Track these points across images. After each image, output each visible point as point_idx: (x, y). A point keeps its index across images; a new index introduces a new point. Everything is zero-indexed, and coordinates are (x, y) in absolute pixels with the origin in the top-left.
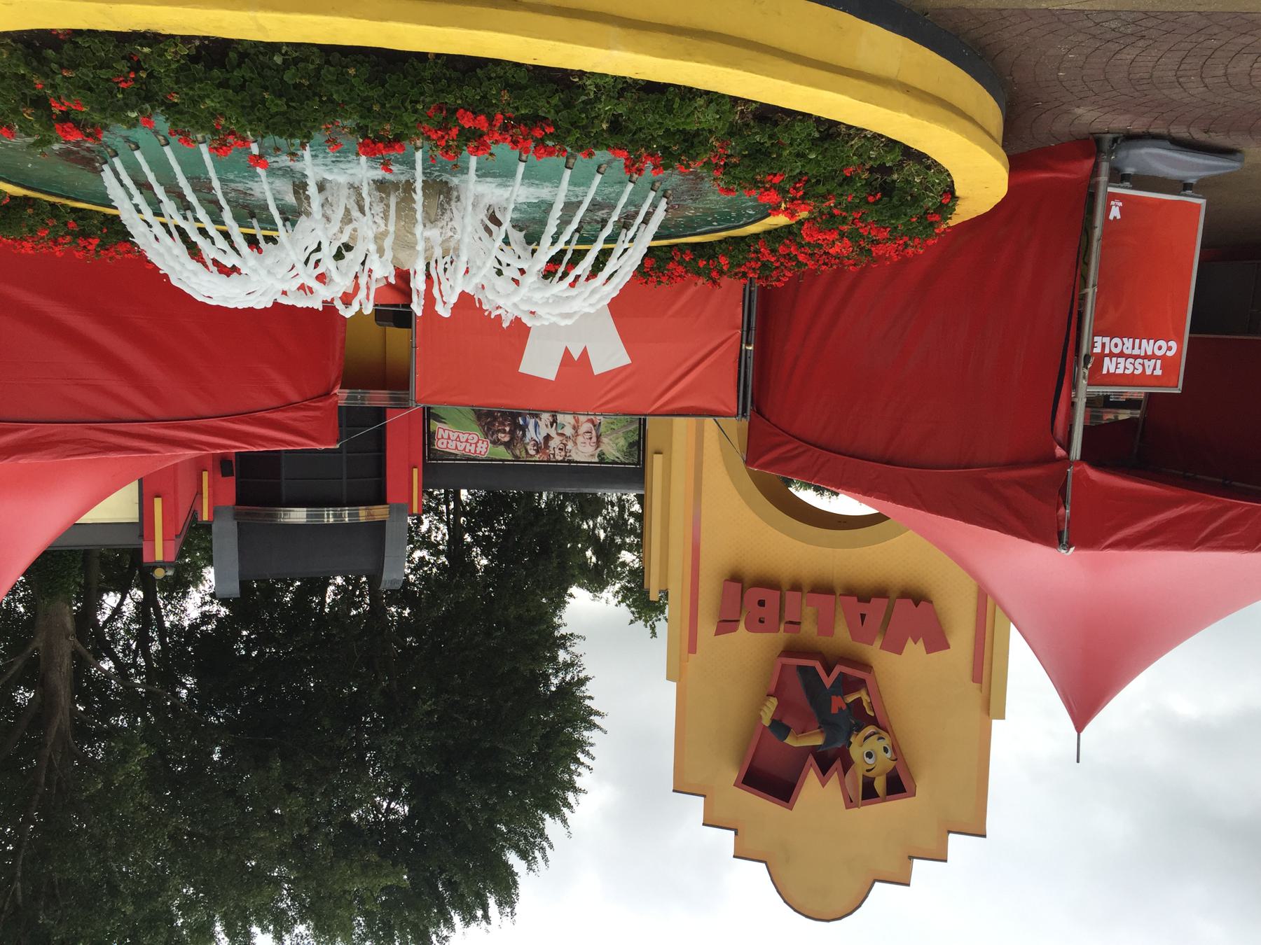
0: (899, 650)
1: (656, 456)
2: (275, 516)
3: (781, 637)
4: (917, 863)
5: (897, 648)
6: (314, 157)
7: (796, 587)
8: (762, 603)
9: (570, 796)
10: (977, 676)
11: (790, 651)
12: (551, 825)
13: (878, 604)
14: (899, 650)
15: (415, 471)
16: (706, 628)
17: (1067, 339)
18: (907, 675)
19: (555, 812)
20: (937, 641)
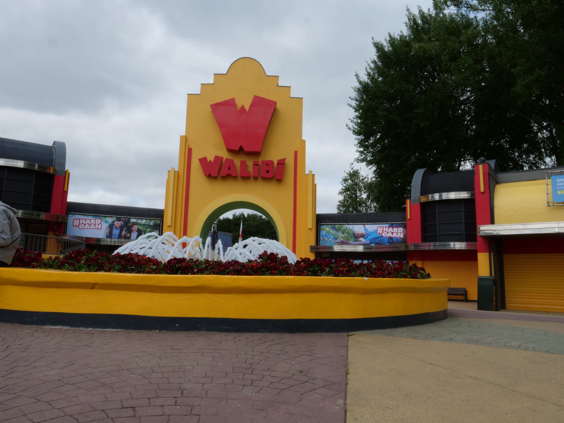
0: (217, 158)
2: (364, 248)
3: (260, 160)
5: (217, 158)
6: (375, 171)
7: (256, 178)
8: (268, 172)
9: (387, 48)
10: (190, 150)
11: (257, 154)
12: (365, 78)
13: (223, 173)
14: (217, 158)
15: (409, 217)
16: (290, 162)
17: (93, 286)
18: (213, 148)
19: (359, 89)
20: (203, 161)
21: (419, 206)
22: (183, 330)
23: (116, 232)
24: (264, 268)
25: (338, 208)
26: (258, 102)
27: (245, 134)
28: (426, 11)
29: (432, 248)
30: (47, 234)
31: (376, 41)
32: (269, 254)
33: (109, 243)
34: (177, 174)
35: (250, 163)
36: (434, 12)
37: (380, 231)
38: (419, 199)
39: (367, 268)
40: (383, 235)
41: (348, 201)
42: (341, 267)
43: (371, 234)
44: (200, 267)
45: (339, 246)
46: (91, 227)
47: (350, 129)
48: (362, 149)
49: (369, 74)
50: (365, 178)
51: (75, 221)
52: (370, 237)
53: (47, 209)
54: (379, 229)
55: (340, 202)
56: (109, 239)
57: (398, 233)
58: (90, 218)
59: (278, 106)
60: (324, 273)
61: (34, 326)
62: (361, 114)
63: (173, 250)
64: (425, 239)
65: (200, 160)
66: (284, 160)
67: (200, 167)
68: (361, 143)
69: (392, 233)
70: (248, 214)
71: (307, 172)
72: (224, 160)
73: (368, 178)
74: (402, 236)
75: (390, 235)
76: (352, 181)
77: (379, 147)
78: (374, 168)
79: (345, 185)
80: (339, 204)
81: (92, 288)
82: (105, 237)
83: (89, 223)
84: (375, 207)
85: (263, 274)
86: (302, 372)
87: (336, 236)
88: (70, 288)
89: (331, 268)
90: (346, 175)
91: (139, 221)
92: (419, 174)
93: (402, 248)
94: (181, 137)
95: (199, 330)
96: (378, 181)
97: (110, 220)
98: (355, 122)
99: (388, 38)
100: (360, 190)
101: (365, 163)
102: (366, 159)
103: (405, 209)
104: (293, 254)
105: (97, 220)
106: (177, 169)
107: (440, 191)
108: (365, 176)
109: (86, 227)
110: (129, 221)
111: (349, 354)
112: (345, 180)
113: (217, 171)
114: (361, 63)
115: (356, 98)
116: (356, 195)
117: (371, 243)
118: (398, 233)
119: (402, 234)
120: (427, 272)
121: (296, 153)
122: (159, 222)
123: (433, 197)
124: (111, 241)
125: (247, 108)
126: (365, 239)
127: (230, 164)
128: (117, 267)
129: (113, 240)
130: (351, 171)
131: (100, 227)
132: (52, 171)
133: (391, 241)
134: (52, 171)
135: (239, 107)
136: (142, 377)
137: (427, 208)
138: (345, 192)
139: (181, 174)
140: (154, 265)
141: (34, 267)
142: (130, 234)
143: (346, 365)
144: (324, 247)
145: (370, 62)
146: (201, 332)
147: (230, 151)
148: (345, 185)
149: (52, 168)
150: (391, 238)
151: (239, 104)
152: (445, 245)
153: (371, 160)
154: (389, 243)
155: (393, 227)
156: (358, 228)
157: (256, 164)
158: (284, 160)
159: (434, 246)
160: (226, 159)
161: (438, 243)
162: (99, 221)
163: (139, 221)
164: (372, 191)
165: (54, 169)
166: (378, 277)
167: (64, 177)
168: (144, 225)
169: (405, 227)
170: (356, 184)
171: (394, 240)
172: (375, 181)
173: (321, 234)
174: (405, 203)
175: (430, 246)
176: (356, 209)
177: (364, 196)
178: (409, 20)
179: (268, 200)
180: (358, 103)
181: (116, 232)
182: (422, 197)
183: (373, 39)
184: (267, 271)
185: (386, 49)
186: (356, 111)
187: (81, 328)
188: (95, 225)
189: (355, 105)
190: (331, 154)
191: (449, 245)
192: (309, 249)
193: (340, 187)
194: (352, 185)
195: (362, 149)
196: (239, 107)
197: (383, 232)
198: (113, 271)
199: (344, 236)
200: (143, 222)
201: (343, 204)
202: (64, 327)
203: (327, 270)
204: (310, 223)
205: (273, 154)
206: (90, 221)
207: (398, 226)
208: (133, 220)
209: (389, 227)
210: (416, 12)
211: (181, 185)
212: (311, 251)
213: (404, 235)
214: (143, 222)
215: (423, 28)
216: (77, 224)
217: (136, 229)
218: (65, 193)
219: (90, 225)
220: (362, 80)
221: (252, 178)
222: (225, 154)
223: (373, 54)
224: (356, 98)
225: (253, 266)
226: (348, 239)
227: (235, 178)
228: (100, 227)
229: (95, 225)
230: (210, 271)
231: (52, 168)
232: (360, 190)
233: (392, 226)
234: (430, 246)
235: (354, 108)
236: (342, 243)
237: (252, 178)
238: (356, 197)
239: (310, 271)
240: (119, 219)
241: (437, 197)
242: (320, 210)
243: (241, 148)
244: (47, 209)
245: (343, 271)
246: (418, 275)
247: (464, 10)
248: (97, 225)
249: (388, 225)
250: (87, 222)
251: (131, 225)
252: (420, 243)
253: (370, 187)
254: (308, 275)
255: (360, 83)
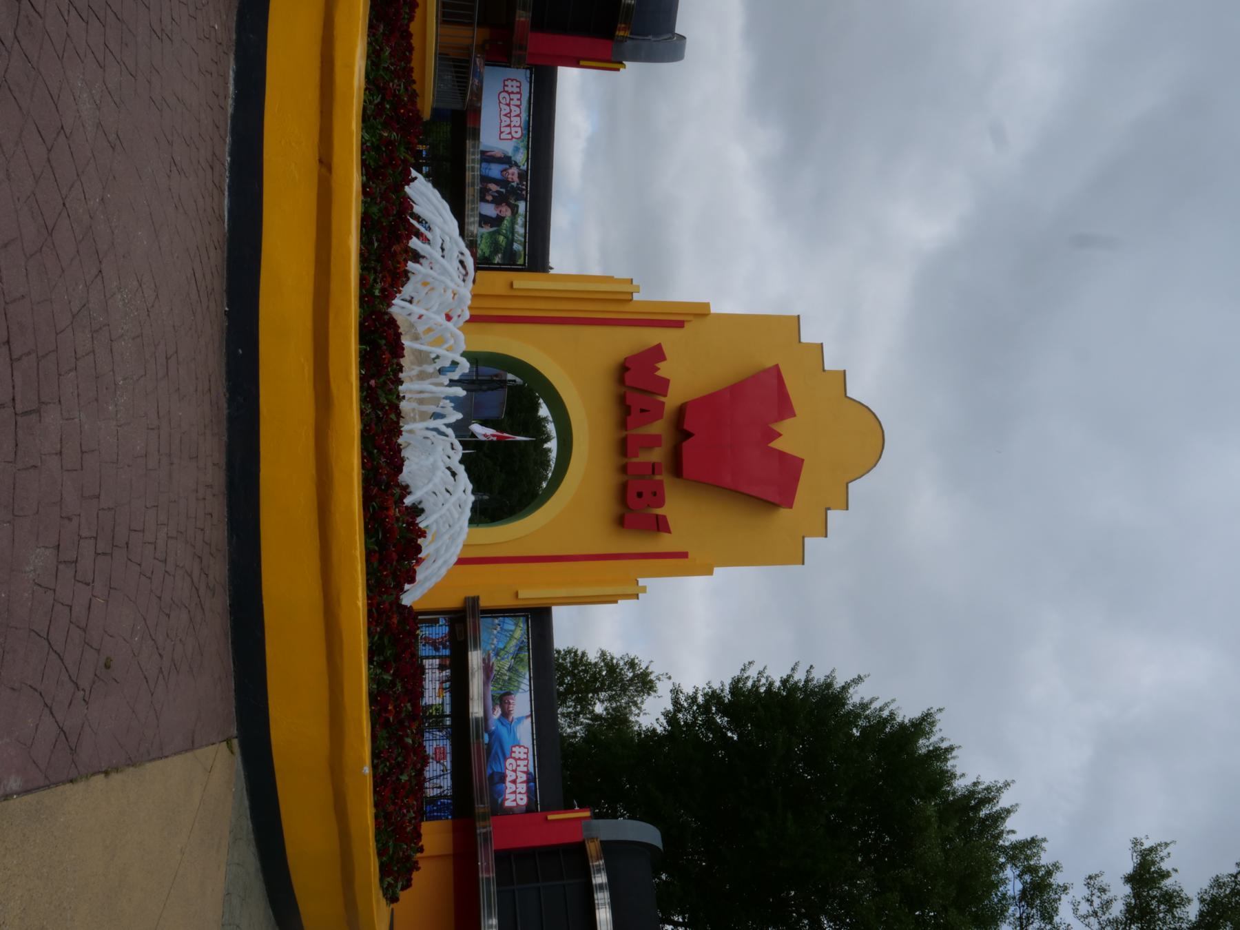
0: (665, 382)
1: (515, 286)
2: (477, 719)
3: (665, 478)
4: (826, 368)
5: (664, 384)
6: (654, 730)
7: (624, 469)
8: (640, 495)
9: (924, 745)
10: (679, 324)
11: (677, 470)
12: (855, 696)
14: (665, 382)
15: (550, 817)
16: (665, 543)
17: (325, 162)
18: (686, 376)
19: (829, 685)
20: (657, 353)
21: (578, 839)
22: (228, 364)
23: (495, 171)
24: (384, 535)
25: (569, 652)
26: (790, 468)
27: (722, 442)
28: (1009, 824)
29: (483, 875)
30: (479, 25)
31: (937, 717)
32: (420, 541)
33: (469, 157)
34: (626, 298)
35: (656, 455)
36: (1007, 844)
37: (519, 752)
38: (592, 839)
39: (399, 764)
40: (510, 761)
41: (586, 671)
42: (395, 707)
43: (510, 731)
44: (380, 392)
45: (480, 661)
46: (504, 118)
47: (743, 670)
48: (700, 700)
49: (864, 706)
50: (639, 708)
51: (515, 83)
52: (503, 731)
53: (538, 24)
54: (523, 750)
55: (583, 654)
56: (478, 157)
57: (515, 795)
58: (524, 116)
59: (784, 512)
60: (379, 671)
61: (234, 37)
62: (778, 694)
63: (433, 316)
64: (503, 858)
65: (659, 348)
66: (668, 530)
67: (642, 349)
68: (713, 697)
69: (514, 782)
70: (549, 450)
71: (642, 582)
72: (662, 399)
73: (638, 715)
74: (508, 804)
75: (510, 776)
76: (632, 680)
77: (707, 737)
78: (659, 730)
79: (622, 663)
80: (579, 653)
81: (321, 161)
82: (482, 148)
83: (513, 114)
84: (574, 735)
85: (369, 532)
86: (107, 666)
87: (502, 653)
88: (322, 112)
89: (393, 684)
90: (643, 666)
91: (520, 221)
92: (649, 834)
93: (480, 808)
94: (707, 305)
95: (231, 401)
96: (632, 739)
97: (521, 158)
98: (759, 681)
99: (944, 745)
100: (611, 698)
101: (670, 707)
102: (680, 711)
103: (570, 808)
104: (455, 559)
105: (519, 130)
106: (636, 297)
107: (612, 886)
108: (643, 707)
109: (503, 107)
110: (520, 197)
111: (169, 759)
112: (632, 664)
113: (636, 383)
114: (888, 687)
115: (812, 680)
116: (601, 689)
117: (490, 735)
118: (515, 795)
119: (514, 804)
120: (403, 895)
121: (684, 555)
122: (521, 261)
123: (599, 871)
124: (473, 161)
125: (777, 444)
126: (499, 719)
127: (652, 412)
128: (375, 209)
129: (477, 166)
130: (652, 677)
131: (503, 136)
132: (622, 33)
133: (496, 779)
134: (622, 33)
135: (778, 427)
136: (75, 310)
137: (573, 857)
138: (607, 665)
139: (628, 307)
140: (383, 290)
141: (372, 28)
142: (492, 202)
143: (132, 763)
144: (476, 629)
145: (892, 707)
146: (225, 405)
147: (681, 411)
148: (622, 663)
149: (627, 34)
150: (503, 778)
151: (784, 426)
152: (489, 907)
153: (677, 721)
154: (492, 776)
155: (527, 782)
156: (522, 704)
157: (654, 468)
158: (667, 530)
159: (488, 879)
160: (663, 404)
161: (493, 889)
162: (519, 135)
163: (520, 221)
164: (610, 727)
165: (625, 39)
166: (375, 792)
167: (609, 60)
168: (513, 231)
169: (530, 809)
170: (624, 690)
171: (499, 787)
172: (633, 731)
173: (507, 620)
174: (582, 807)
175: (487, 872)
176: (569, 690)
177: (599, 709)
178: (988, 789)
179: (578, 499)
180: (801, 685)
181: (495, 171)
182: (597, 843)
183: (940, 710)
184: (378, 543)
185: (921, 742)
186: (784, 682)
187: (228, 140)
188: (509, 126)
189: (796, 678)
190: (687, 632)
191: (490, 916)
192: (472, 594)
193: (617, 651)
194: (622, 680)
195: (700, 700)
196: (778, 427)
197: (516, 760)
198: (364, 202)
199: (504, 671)
200: (520, 229)
201: (578, 660)
202: (230, 101)
203: (388, 677)
204: (531, 595)
205: (680, 507)
206: (518, 116)
207: (530, 793)
208: (522, 206)
209: (527, 773)
210: (1004, 801)
211: (602, 307)
212: (466, 599)
213: (511, 808)
214: (520, 229)
215: (971, 821)
216: (509, 89)
217: (503, 215)
218: (574, 62)
219: (508, 115)
220: (851, 690)
221: (625, 460)
222: (672, 400)
223: (907, 713)
224: (812, 680)
225: (388, 509)
226: (497, 681)
227: (623, 424)
228: (503, 136)
229: (509, 126)
230: (373, 416)
231: (627, 34)
232: (611, 698)
233: (530, 779)
234: (487, 872)
235: (789, 676)
236: (487, 669)
237: (625, 460)
238: (596, 691)
239: (380, 638)
240: (522, 176)
241: (600, 879)
242: (560, 616)
243: (688, 435)
244: (538, 24)
245: (386, 710)
246: (390, 880)
247: (1013, 911)
248: (508, 130)
249: (531, 770)
250: (513, 108)
251: (512, 201)
252: (493, 847)
253: (619, 719)
254: (370, 634)
255: (845, 688)
